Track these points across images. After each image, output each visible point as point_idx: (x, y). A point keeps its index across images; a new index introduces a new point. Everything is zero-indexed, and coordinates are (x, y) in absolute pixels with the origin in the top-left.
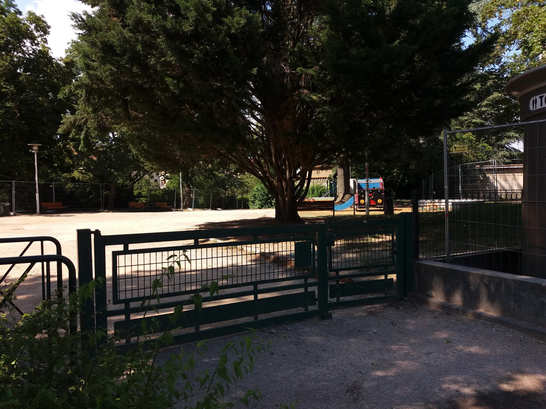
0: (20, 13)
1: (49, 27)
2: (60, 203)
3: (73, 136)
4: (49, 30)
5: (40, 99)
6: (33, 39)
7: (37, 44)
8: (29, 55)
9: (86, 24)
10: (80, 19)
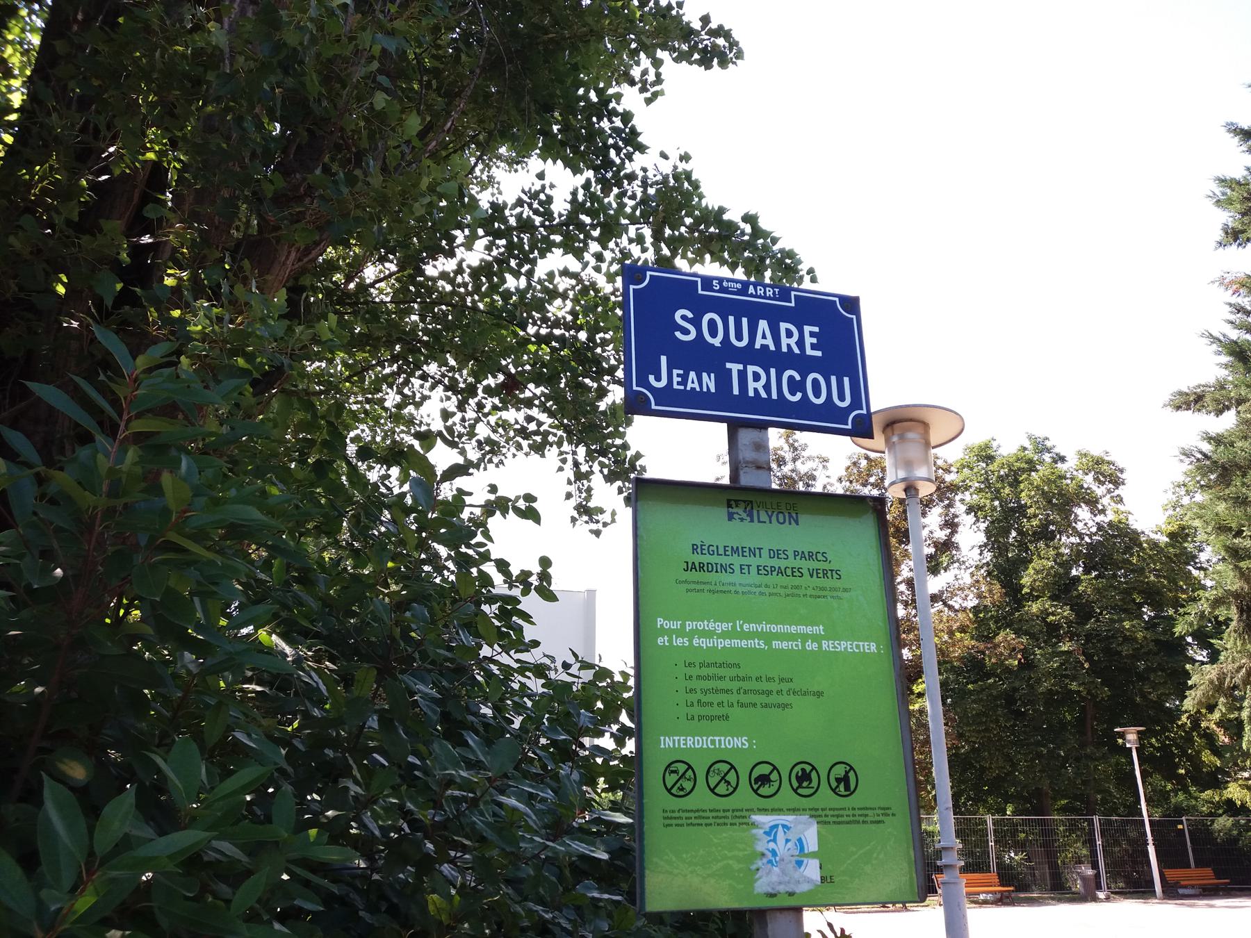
0: (1062, 459)
1: (1122, 471)
2: (1208, 871)
3: (1223, 715)
4: (1123, 476)
5: (1127, 624)
6: (1092, 502)
7: (1103, 512)
8: (1090, 536)
9: (1216, 462)
10: (1200, 456)
